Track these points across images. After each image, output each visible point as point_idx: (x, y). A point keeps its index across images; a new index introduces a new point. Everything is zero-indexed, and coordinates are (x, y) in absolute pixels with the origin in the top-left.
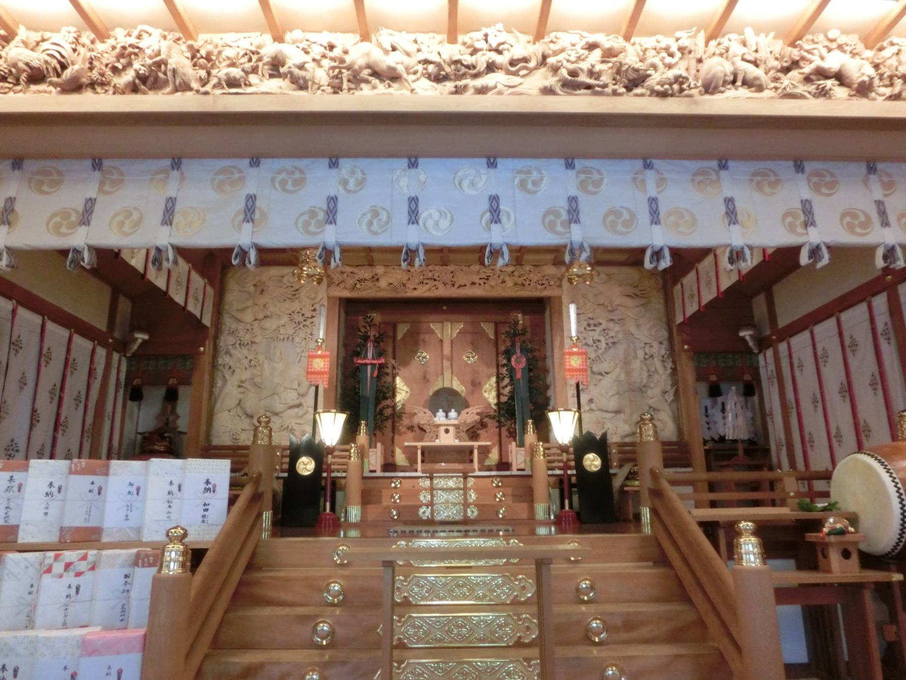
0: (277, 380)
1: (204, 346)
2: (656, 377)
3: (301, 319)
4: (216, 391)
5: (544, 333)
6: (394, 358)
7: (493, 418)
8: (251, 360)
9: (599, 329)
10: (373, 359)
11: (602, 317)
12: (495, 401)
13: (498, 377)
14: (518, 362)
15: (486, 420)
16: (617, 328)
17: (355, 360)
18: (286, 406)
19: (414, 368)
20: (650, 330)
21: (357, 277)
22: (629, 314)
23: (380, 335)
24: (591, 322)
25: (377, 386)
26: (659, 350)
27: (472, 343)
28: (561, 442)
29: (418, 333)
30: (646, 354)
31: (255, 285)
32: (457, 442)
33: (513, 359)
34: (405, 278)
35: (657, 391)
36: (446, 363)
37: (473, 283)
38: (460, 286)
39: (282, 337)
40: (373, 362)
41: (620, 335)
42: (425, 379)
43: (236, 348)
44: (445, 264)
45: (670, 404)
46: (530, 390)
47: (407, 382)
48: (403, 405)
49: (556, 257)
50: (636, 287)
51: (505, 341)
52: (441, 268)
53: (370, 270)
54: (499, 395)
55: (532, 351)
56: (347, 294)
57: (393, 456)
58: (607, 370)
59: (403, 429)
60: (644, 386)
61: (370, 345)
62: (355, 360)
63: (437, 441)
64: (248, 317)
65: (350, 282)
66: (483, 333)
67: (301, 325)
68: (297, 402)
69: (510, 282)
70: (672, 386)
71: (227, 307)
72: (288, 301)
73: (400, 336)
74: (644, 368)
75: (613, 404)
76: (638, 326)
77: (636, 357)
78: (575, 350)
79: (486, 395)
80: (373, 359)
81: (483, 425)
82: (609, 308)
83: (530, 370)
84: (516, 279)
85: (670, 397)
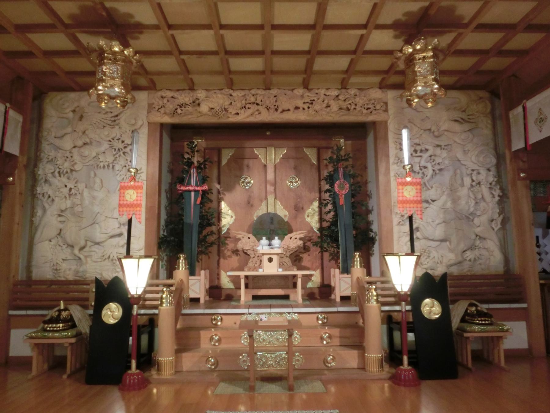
0: (96, 209)
1: (12, 175)
2: (482, 204)
3: (121, 146)
4: (36, 220)
5: (365, 158)
6: (219, 183)
7: (315, 244)
8: (71, 189)
9: (426, 155)
10: (197, 185)
11: (428, 142)
12: (318, 226)
13: (321, 204)
14: (341, 187)
15: (308, 244)
16: (444, 154)
17: (178, 187)
18: (106, 236)
19: (238, 194)
20: (477, 156)
21: (177, 102)
22: (457, 140)
23: (205, 161)
24: (418, 148)
25: (201, 212)
26: (487, 177)
27: (295, 168)
28: (399, 289)
29: (243, 159)
30: (473, 181)
31: (74, 111)
32: (280, 272)
33: (336, 185)
34: (227, 103)
35: (484, 218)
36: (270, 188)
37: (297, 108)
38: (283, 111)
39: (102, 164)
40: (196, 188)
41: (447, 162)
42: (250, 204)
43: (55, 177)
44: (268, 88)
45: (496, 233)
46: (354, 215)
47: (232, 206)
48: (228, 229)
49: (383, 79)
50: (464, 111)
51: (327, 165)
52: (263, 92)
53: (192, 94)
54: (321, 220)
55: (353, 176)
56: (167, 120)
57: (219, 279)
58: (434, 198)
59: (228, 253)
60: (471, 214)
61: (193, 171)
62: (178, 187)
63: (260, 270)
64: (67, 143)
65: (170, 107)
66: (305, 158)
67: (121, 153)
68: (118, 231)
69: (334, 107)
70: (500, 214)
71: (45, 133)
72: (108, 128)
73: (224, 162)
74: (471, 195)
75: (439, 233)
76: (465, 152)
77: (463, 185)
78: (408, 179)
79: (308, 219)
80: (197, 185)
81: (305, 249)
82: (436, 134)
83: (353, 196)
84: (341, 102)
85: (497, 225)
